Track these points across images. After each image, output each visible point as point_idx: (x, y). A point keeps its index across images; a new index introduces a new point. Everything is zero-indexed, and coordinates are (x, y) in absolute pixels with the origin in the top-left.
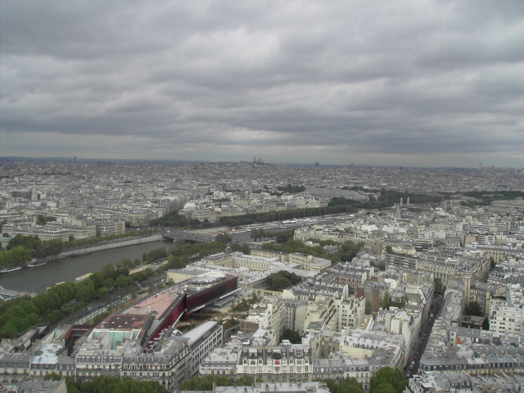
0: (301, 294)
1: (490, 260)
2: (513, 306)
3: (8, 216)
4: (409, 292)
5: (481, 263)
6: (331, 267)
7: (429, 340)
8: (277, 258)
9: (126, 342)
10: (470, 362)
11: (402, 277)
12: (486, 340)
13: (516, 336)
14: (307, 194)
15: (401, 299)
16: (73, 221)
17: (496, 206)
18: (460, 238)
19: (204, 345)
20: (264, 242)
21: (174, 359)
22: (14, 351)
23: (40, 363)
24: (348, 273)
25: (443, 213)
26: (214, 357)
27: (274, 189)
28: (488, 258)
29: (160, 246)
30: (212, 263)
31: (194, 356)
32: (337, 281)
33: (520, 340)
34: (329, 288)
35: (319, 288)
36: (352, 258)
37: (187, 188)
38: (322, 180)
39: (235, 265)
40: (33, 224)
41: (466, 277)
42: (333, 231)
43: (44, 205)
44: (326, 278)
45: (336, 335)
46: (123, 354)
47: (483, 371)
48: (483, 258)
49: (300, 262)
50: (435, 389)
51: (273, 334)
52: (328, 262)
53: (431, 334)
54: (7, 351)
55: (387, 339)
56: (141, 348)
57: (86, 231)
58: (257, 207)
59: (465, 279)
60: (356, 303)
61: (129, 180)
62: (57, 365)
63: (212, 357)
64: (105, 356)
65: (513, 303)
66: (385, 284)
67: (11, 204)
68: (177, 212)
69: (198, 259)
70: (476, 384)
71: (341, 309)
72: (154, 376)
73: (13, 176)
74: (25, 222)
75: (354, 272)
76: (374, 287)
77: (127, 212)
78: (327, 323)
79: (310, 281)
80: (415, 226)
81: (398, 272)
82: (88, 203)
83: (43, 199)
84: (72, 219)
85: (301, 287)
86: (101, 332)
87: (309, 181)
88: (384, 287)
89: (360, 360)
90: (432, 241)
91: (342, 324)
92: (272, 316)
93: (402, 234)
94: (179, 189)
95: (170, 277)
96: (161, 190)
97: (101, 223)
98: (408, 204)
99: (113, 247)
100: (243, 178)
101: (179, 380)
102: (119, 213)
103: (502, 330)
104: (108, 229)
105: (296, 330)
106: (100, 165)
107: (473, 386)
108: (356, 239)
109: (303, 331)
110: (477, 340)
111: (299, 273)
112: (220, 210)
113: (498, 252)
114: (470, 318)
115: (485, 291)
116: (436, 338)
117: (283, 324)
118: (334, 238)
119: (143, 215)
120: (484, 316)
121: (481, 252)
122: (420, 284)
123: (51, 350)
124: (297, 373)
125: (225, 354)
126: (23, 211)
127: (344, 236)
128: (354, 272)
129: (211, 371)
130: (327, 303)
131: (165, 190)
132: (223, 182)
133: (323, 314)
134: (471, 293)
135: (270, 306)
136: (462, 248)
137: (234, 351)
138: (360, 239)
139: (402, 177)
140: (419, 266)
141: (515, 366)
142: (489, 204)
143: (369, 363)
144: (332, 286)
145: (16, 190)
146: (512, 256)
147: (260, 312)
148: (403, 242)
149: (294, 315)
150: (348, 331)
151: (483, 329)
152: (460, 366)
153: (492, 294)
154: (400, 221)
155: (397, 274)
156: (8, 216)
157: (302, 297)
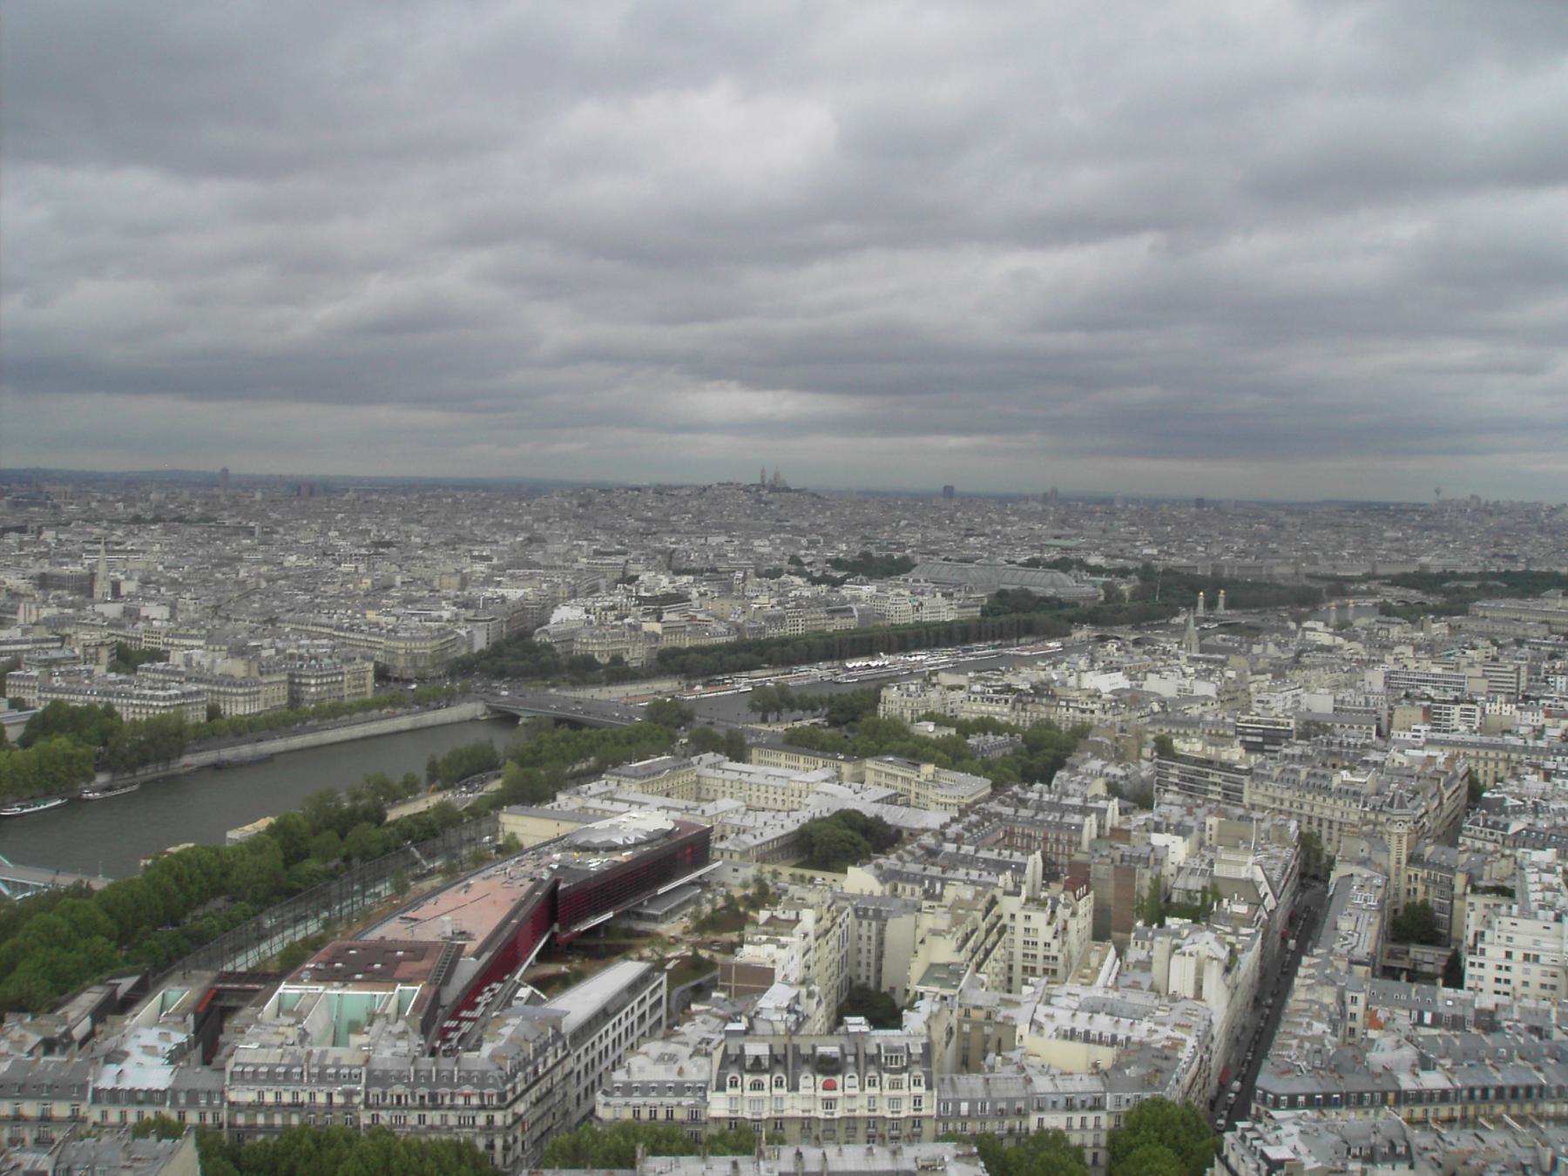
0: (901, 880)
1: (1466, 779)
2: (1535, 915)
3: (25, 647)
4: (1224, 874)
5: (1439, 788)
6: (990, 798)
7: (1284, 1019)
8: (828, 772)
9: (378, 1024)
10: (1407, 1083)
11: (1203, 830)
12: (1454, 1017)
13: (1545, 1005)
14: (919, 581)
15: (1199, 895)
16: (219, 661)
17: (1485, 617)
18: (1375, 712)
19: (610, 1031)
20: (790, 726)
21: (520, 1074)
22: (41, 1051)
23: (120, 1087)
24: (1040, 817)
25: (1325, 638)
26: (641, 1069)
27: (820, 566)
28: (1461, 771)
29: (479, 736)
30: (634, 787)
31: (581, 1066)
32: (1009, 839)
33: (1557, 1019)
34: (986, 861)
35: (955, 862)
36: (1054, 773)
37: (559, 563)
38: (962, 540)
39: (704, 792)
40: (100, 670)
41: (1396, 829)
42: (995, 692)
43: (132, 615)
44: (975, 831)
45: (1006, 1003)
46: (368, 1060)
47: (1444, 1112)
48: (1447, 773)
49: (899, 784)
50: (1302, 1165)
51: (816, 999)
52: (982, 785)
53: (1290, 1001)
54: (21, 1050)
55: (1158, 1013)
56: (422, 1042)
57: (258, 692)
58: (769, 619)
59: (1390, 834)
60: (1066, 906)
61: (388, 537)
62: (169, 1093)
63: (634, 1069)
64: (314, 1066)
65: (1534, 906)
66: (1153, 850)
67: (34, 612)
68: (531, 634)
69: (594, 774)
70: (1426, 1149)
71: (1020, 924)
72: (460, 1126)
73: (39, 528)
74: (75, 664)
75: (1058, 815)
76: (1118, 858)
77: (380, 635)
78: (979, 966)
79: (928, 840)
80: (1241, 676)
81: (1190, 813)
82: (262, 606)
83: (129, 595)
84: (217, 654)
85: (900, 858)
86: (301, 995)
87: (924, 543)
88: (1148, 858)
89: (1077, 1077)
90: (1292, 722)
91: (1025, 969)
92: (814, 945)
93: (1204, 700)
94: (537, 565)
95: (508, 829)
96: (480, 567)
97: (302, 666)
98: (1221, 609)
99: (339, 739)
100: (727, 533)
101: (534, 1138)
102: (357, 636)
103: (1503, 987)
104: (322, 684)
105: (885, 988)
106: (299, 495)
107: (1415, 1156)
108: (1064, 716)
109: (907, 991)
110: (1428, 1017)
111: (893, 816)
112: (657, 628)
113: (1492, 754)
114: (1407, 953)
115: (1451, 870)
116: (1305, 1010)
117: (846, 970)
118: (1001, 712)
119: (428, 645)
120: (1449, 946)
121: (1441, 756)
122: (1256, 850)
123: (154, 1048)
124: (889, 1115)
125: (673, 1058)
126: (67, 631)
127: (1029, 707)
128: (1058, 815)
129: (631, 1109)
130: (979, 907)
131: (493, 568)
132: (668, 545)
133: (966, 939)
134: (1410, 877)
135: (808, 917)
136: (1381, 743)
137: (701, 1050)
138: (1078, 714)
139: (1203, 531)
140: (1255, 797)
141: (1541, 1095)
142: (1463, 612)
143: (1104, 1085)
144: (993, 855)
145: (47, 568)
146: (1531, 765)
147: (777, 934)
148: (1207, 723)
149: (881, 943)
150: (1040, 990)
151: (1445, 985)
152: (1378, 1096)
153: (1471, 879)
154: (1197, 660)
155: (1189, 821)
156: (25, 647)
157: (904, 889)
